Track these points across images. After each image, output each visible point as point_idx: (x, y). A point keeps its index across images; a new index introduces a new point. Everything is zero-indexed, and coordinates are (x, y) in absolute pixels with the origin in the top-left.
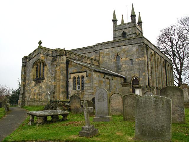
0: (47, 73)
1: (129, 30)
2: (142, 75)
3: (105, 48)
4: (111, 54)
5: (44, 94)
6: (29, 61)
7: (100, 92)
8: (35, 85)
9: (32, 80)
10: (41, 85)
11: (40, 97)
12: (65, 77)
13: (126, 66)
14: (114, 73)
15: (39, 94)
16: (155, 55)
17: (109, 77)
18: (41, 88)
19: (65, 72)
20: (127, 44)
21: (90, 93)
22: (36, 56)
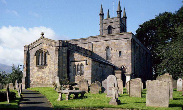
0: (50, 61)
1: (114, 24)
2: (129, 65)
3: (98, 40)
4: (102, 46)
5: (47, 78)
6: (31, 49)
7: (110, 78)
8: (38, 71)
9: (35, 66)
10: (43, 70)
11: (43, 81)
12: (67, 65)
13: (115, 57)
14: (104, 62)
15: (42, 78)
16: (140, 48)
17: (103, 65)
18: (44, 73)
19: (66, 60)
20: (117, 38)
21: (89, 78)
22: (38, 45)
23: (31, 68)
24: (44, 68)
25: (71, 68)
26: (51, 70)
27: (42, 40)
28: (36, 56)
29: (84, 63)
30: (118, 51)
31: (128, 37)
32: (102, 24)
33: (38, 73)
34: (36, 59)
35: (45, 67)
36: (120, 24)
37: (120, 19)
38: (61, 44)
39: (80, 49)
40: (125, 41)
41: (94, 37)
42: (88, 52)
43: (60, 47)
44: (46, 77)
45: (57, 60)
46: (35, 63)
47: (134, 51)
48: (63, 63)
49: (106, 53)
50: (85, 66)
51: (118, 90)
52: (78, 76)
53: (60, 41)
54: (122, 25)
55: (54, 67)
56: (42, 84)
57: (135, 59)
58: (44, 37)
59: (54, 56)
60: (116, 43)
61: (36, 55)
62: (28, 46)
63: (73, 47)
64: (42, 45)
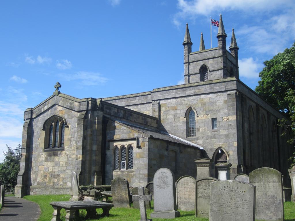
0: (70, 140)
2: (232, 146)
4: (179, 108)
5: (62, 176)
7: (161, 175)
8: (46, 160)
10: (57, 159)
11: (56, 180)
12: (100, 147)
13: (204, 129)
15: (53, 175)
16: (258, 110)
18: (57, 164)
21: (143, 176)
23: (34, 154)
24: (57, 155)
25: (109, 153)
26: (70, 159)
27: (57, 98)
28: (44, 132)
29: (134, 143)
30: (209, 117)
31: (229, 88)
32: (189, 63)
33: (45, 163)
34: (43, 136)
35: (59, 152)
36: (224, 62)
37: (223, 52)
38: (90, 105)
39: (131, 115)
40: (224, 97)
41: (163, 89)
42: (149, 120)
43: (87, 111)
44: (60, 173)
45: (82, 139)
46: (42, 145)
47: (243, 117)
48: (92, 145)
49: (187, 123)
50: (136, 150)
51: (150, 201)
52: (122, 171)
53: (87, 99)
54: (229, 64)
55: (75, 152)
56: (53, 187)
57: (246, 132)
58: (59, 93)
59: (76, 129)
60: (205, 100)
61: (43, 129)
62: (32, 112)
63: (116, 110)
64: (56, 109)
